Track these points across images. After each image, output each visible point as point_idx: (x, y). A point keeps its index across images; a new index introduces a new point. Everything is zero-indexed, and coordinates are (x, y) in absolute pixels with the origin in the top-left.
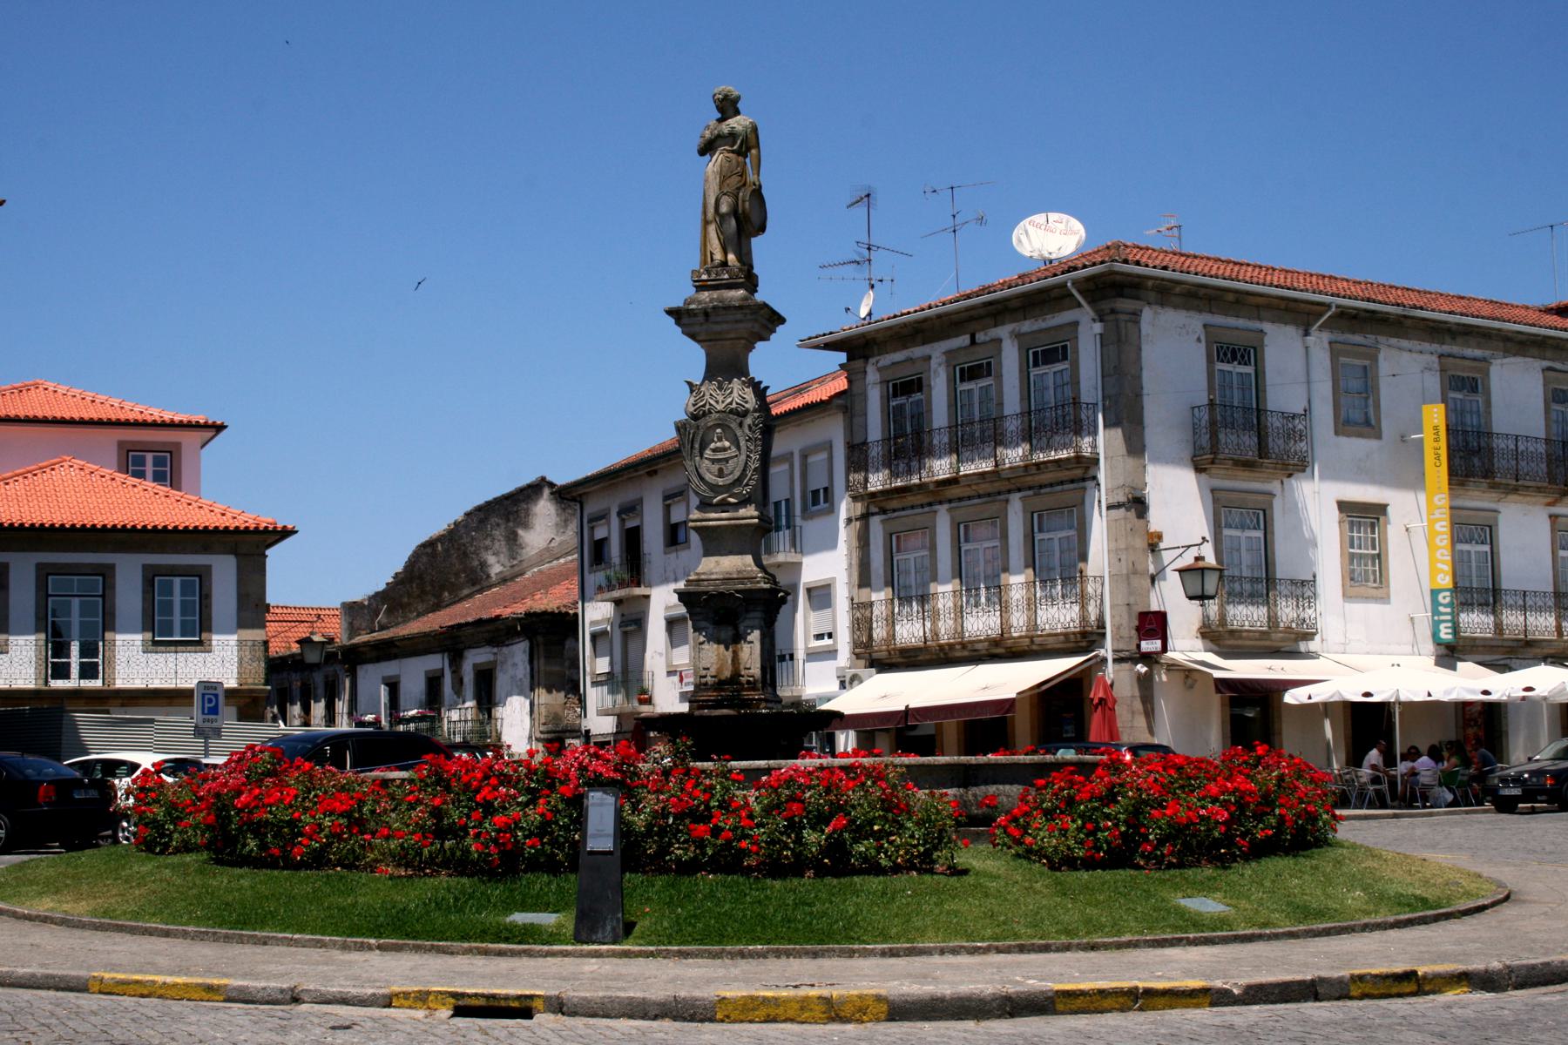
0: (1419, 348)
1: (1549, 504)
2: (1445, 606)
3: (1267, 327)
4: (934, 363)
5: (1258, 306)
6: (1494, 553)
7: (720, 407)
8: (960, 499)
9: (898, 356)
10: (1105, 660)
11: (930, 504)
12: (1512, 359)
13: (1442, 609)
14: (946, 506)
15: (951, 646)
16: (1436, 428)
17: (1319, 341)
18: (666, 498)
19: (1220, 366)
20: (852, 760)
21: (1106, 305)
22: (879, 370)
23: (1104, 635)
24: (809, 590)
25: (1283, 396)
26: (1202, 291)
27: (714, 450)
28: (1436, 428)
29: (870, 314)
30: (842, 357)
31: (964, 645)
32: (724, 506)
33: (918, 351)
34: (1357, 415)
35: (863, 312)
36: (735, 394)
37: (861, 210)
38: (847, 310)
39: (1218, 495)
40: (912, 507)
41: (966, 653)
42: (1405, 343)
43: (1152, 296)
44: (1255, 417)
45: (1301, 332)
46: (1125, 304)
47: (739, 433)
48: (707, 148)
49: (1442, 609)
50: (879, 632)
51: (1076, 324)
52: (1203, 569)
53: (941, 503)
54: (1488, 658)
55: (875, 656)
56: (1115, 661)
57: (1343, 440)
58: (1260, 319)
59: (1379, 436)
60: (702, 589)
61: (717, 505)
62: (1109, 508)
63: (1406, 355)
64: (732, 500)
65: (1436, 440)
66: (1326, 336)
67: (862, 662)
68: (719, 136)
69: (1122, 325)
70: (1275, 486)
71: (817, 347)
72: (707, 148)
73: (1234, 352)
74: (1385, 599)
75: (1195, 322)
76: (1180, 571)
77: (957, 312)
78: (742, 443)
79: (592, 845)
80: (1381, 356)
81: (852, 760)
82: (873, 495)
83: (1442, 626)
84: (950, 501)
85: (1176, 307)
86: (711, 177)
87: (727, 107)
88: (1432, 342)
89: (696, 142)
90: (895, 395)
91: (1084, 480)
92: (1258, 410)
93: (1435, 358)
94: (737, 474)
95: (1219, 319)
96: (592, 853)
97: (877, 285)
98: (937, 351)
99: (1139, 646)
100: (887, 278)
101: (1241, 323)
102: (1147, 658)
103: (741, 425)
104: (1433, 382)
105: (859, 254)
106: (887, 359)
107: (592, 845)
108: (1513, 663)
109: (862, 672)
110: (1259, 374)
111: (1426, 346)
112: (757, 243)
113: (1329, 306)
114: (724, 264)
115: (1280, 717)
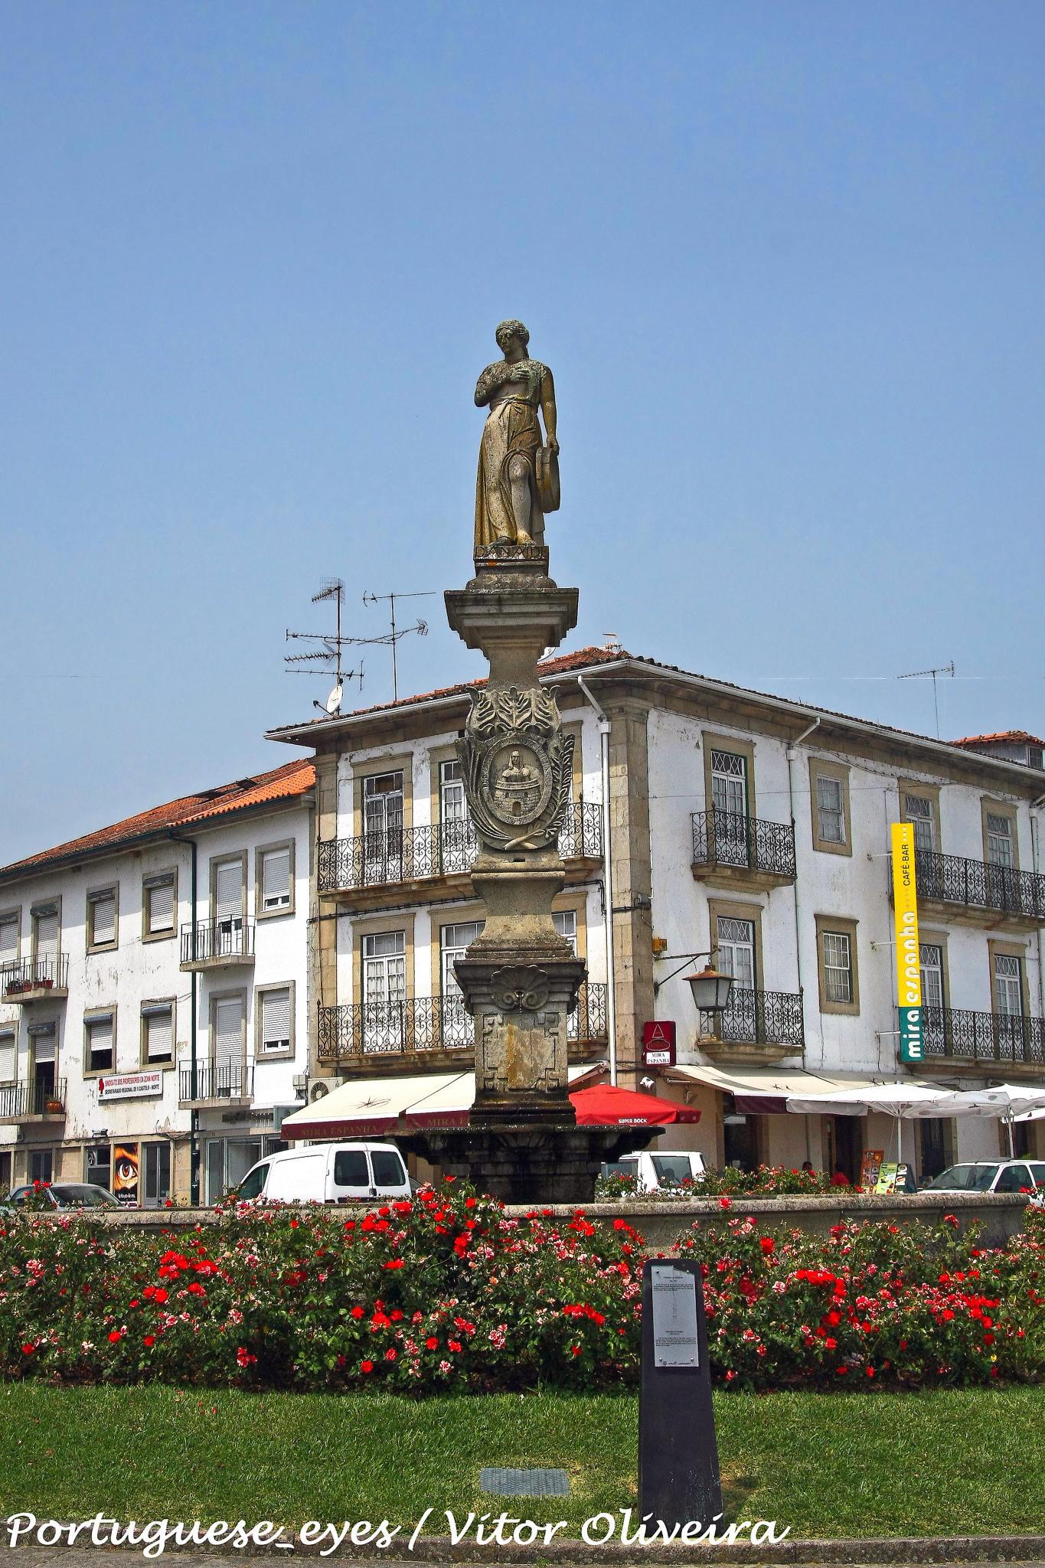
0: (881, 769)
1: (988, 928)
2: (914, 1024)
3: (756, 738)
4: (416, 760)
5: (749, 717)
6: (943, 973)
7: (516, 724)
8: (443, 901)
9: (376, 752)
10: (608, 1071)
11: (408, 906)
12: (958, 787)
13: (910, 1027)
14: (427, 908)
15: (432, 1054)
16: (904, 847)
17: (800, 755)
18: (90, 896)
19: (716, 774)
20: (738, 1204)
21: (614, 703)
22: (353, 766)
23: (607, 1045)
24: (262, 994)
25: (770, 809)
26: (702, 696)
27: (508, 779)
28: (904, 847)
29: (338, 709)
30: (310, 752)
31: (447, 1054)
32: (518, 851)
33: (399, 748)
34: (830, 832)
35: (331, 708)
36: (533, 708)
37: (331, 603)
38: (316, 703)
39: (716, 906)
40: (388, 909)
41: (448, 1063)
42: (871, 764)
43: (657, 697)
44: (746, 829)
45: (785, 745)
46: (636, 703)
47: (543, 757)
48: (488, 397)
49: (910, 1027)
50: (346, 1039)
51: (580, 723)
52: (717, 979)
53: (420, 904)
54: (940, 1077)
55: (343, 1064)
56: (617, 1071)
57: (821, 856)
58: (750, 729)
59: (850, 856)
60: (492, 961)
61: (512, 850)
62: (614, 911)
63: (871, 776)
64: (529, 845)
65: (904, 859)
66: (806, 753)
67: (327, 1071)
68: (508, 382)
69: (631, 724)
70: (761, 899)
71: (283, 739)
72: (488, 397)
73: (725, 759)
74: (857, 1014)
75: (695, 728)
76: (692, 980)
77: (445, 707)
78: (546, 765)
79: (663, 1357)
80: (851, 774)
81: (738, 1204)
82: (346, 893)
83: (911, 1044)
84: (431, 903)
85: (678, 712)
86: (496, 433)
87: (514, 341)
88: (892, 765)
89: (470, 391)
90: (370, 792)
91: (585, 883)
92: (747, 817)
93: (895, 781)
94: (539, 811)
95: (714, 728)
96: (665, 1370)
97: (345, 679)
98: (420, 748)
99: (644, 1058)
100: (357, 672)
101: (733, 732)
102: (654, 1071)
103: (545, 747)
104: (894, 802)
105: (330, 649)
106: (360, 756)
107: (663, 1357)
108: (962, 1084)
109: (329, 1082)
110: (749, 783)
111: (888, 769)
112: (548, 518)
113: (813, 720)
114: (513, 541)
115: (767, 1134)
